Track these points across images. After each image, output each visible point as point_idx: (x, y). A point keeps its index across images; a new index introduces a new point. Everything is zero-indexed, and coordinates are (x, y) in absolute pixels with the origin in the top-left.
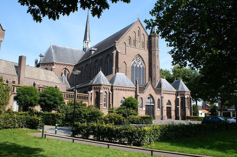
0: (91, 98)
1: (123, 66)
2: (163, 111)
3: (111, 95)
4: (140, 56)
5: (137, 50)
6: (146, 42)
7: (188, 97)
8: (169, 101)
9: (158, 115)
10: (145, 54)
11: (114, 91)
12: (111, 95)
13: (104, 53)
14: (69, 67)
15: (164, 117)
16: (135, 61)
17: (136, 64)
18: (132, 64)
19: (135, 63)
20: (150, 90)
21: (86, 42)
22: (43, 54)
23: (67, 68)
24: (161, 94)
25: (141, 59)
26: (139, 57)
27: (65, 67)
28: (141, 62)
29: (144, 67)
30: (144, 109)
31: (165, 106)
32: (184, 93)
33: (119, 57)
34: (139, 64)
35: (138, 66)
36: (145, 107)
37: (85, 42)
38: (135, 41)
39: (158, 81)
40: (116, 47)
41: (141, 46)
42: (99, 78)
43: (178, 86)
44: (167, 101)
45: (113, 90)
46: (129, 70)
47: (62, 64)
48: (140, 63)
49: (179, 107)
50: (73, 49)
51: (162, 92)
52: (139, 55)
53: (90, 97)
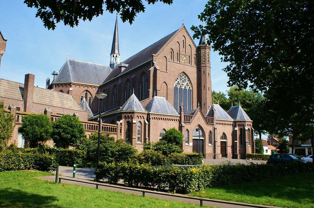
0: (121, 130)
1: (162, 88)
2: (216, 147)
3: (147, 126)
4: (186, 74)
5: (182, 66)
6: (194, 56)
7: (249, 129)
8: (224, 133)
9: (209, 152)
10: (192, 71)
11: (151, 120)
12: (147, 126)
13: (138, 71)
14: (92, 88)
15: (217, 155)
16: (179, 81)
17: (180, 85)
18: (175, 85)
19: (178, 83)
20: (198, 119)
21: (113, 56)
22: (57, 72)
23: (88, 89)
24: (213, 124)
25: (187, 78)
26: (184, 76)
27: (86, 88)
28: (187, 82)
29: (191, 89)
30: (191, 144)
31: (219, 140)
32: (243, 123)
33: (158, 75)
34: (185, 85)
35: (183, 88)
36: (192, 141)
37: (112, 56)
38: (179, 54)
39: (210, 108)
40: (154, 62)
41: (187, 61)
42: (131, 103)
43: (236, 114)
44: (221, 134)
45: (150, 119)
46: (171, 92)
47: (83, 85)
48: (185, 84)
49: (237, 141)
50: (96, 65)
51: (215, 122)
52: (184, 72)
53: (119, 128)
